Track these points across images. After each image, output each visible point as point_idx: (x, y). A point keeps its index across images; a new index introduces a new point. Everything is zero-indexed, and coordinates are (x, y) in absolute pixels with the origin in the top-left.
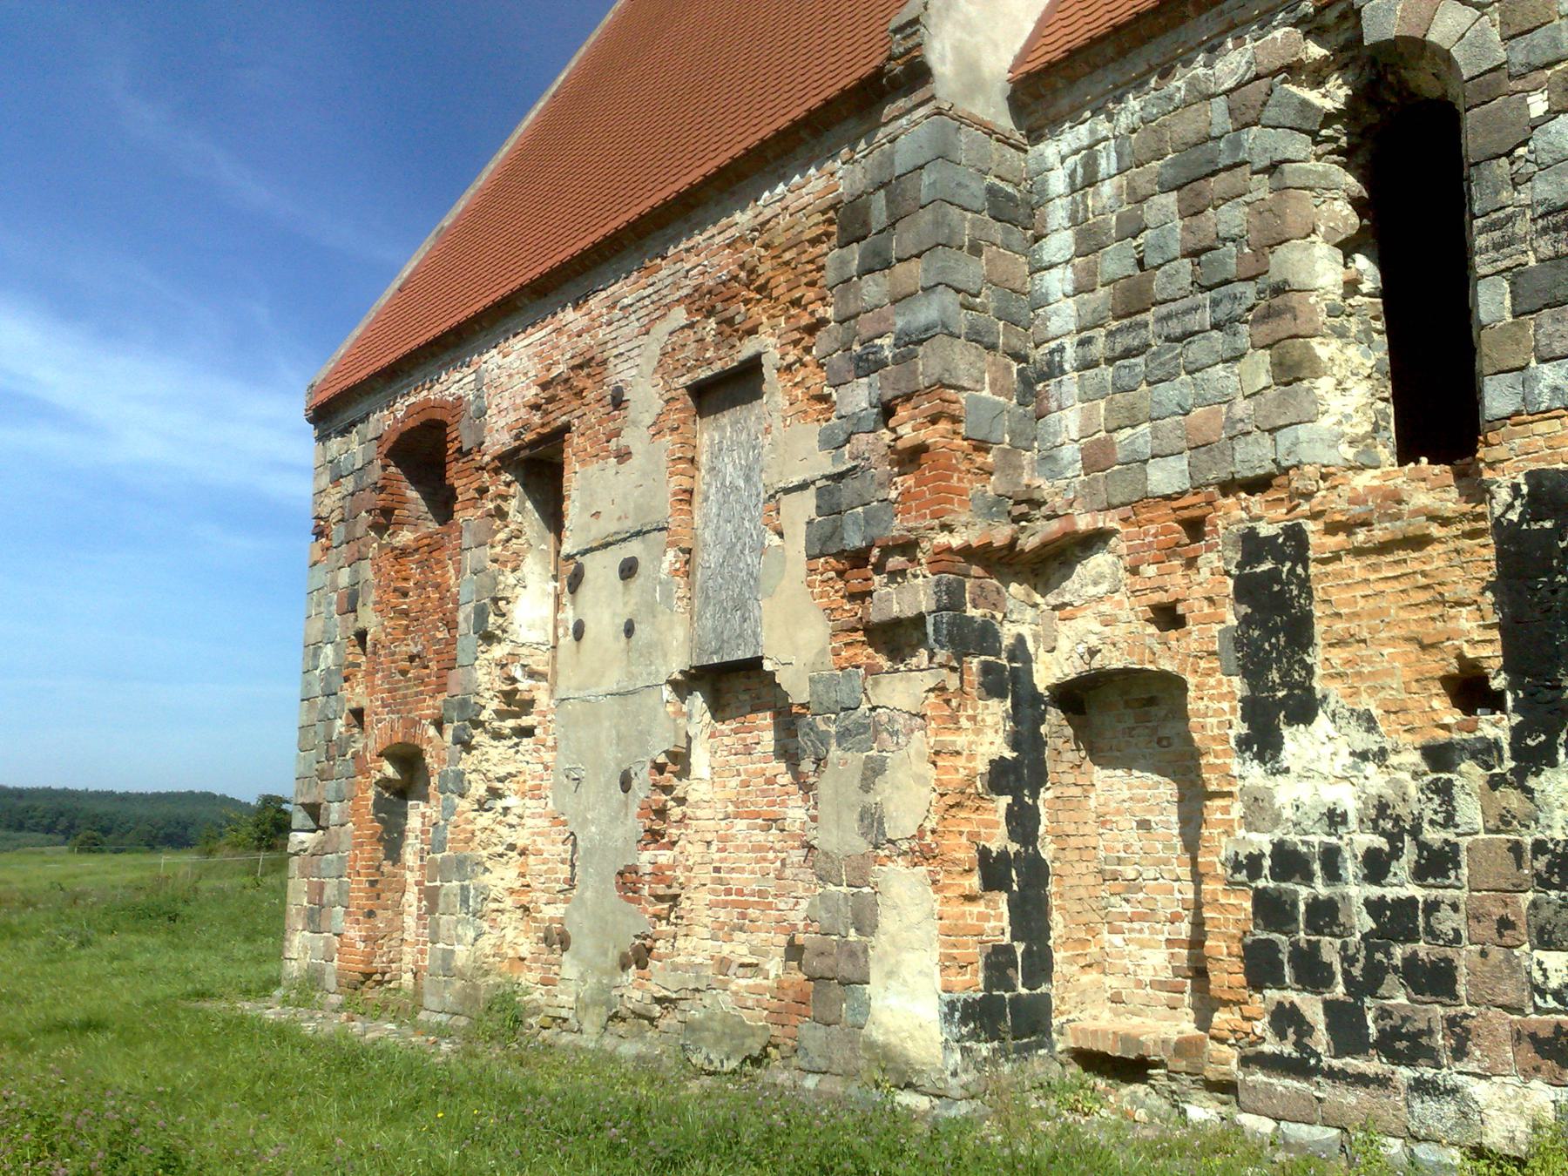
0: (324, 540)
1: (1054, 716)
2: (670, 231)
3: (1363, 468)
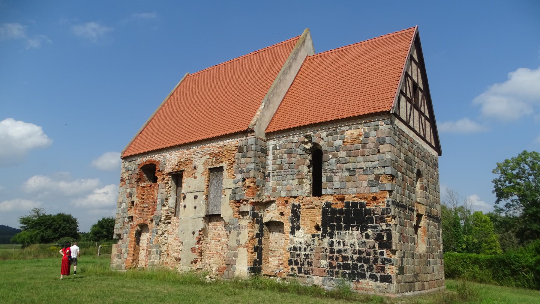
0: (123, 182)
1: (265, 226)
2: (207, 142)
3: (308, 197)
